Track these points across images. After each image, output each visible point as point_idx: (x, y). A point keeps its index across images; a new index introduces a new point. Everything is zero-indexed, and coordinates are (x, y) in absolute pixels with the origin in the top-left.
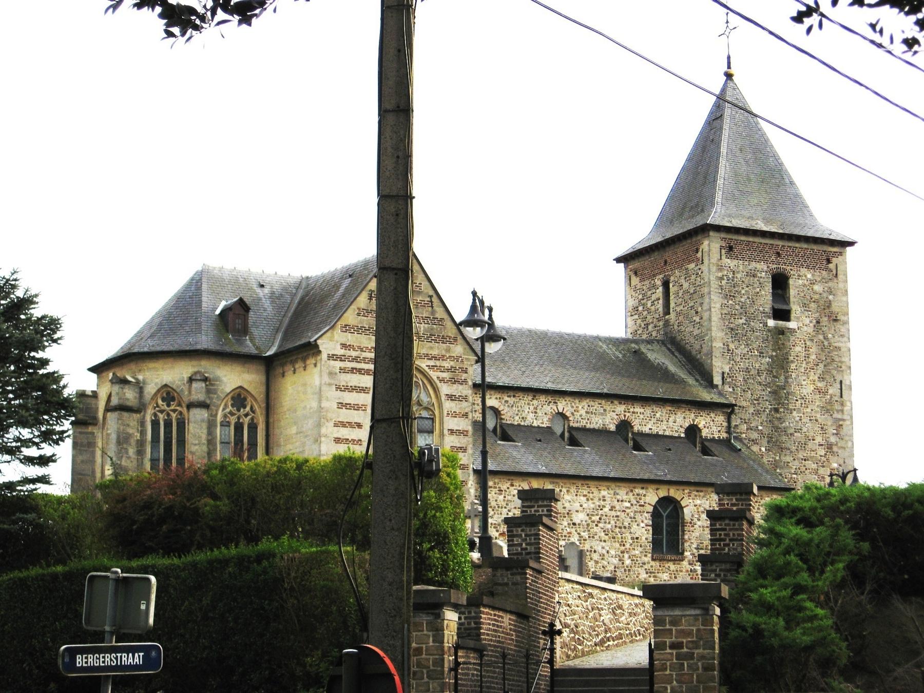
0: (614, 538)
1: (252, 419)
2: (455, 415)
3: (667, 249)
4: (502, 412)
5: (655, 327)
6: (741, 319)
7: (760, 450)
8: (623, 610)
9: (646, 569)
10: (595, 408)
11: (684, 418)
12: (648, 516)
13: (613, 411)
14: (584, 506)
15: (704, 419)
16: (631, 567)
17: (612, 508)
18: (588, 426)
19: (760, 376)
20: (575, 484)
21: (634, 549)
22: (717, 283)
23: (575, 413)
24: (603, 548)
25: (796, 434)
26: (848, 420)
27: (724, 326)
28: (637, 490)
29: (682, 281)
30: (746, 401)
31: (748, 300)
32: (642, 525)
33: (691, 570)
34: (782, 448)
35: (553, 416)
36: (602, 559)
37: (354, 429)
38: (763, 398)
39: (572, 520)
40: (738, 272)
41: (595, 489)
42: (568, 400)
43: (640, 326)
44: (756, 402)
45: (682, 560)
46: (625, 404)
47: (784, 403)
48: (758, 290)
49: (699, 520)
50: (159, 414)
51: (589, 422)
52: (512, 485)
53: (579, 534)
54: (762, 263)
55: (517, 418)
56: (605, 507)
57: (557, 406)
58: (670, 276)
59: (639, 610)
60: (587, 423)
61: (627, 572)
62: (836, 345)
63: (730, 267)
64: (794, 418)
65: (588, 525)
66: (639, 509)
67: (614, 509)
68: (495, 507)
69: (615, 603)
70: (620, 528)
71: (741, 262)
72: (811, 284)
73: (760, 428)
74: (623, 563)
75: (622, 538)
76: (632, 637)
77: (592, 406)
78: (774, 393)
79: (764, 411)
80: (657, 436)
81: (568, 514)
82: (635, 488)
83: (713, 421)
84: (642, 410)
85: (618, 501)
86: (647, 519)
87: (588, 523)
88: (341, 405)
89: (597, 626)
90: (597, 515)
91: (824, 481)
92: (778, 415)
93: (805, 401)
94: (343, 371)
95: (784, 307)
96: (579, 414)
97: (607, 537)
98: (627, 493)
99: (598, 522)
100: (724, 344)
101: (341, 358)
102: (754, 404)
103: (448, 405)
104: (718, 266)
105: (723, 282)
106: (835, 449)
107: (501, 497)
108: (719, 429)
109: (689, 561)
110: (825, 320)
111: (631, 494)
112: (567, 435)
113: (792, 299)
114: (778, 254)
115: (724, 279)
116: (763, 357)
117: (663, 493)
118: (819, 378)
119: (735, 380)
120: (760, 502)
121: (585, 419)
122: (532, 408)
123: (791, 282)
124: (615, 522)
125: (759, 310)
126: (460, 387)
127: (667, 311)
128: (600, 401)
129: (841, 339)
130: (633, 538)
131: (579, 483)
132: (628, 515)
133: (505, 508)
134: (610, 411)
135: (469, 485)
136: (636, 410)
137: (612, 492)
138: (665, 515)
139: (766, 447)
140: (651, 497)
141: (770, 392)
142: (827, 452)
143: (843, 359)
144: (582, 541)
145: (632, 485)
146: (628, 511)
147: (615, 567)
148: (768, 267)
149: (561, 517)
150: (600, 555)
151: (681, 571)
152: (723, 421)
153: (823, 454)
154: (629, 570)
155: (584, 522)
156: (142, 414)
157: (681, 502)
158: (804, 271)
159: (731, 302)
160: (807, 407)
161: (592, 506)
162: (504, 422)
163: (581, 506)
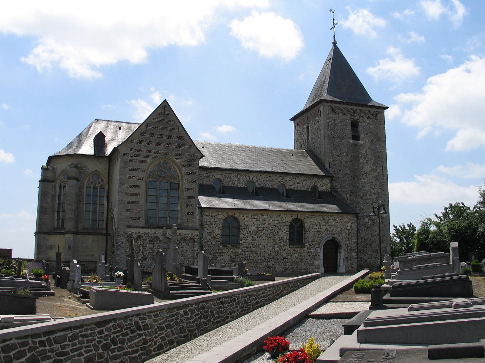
1: (102, 185)
3: (308, 113)
4: (223, 181)
5: (304, 145)
6: (338, 140)
7: (347, 196)
9: (286, 252)
14: (255, 223)
17: (269, 224)
18: (264, 186)
22: (326, 124)
25: (363, 189)
26: (386, 182)
29: (313, 125)
32: (284, 231)
37: (136, 188)
40: (336, 120)
43: (299, 146)
45: (304, 247)
50: (62, 183)
53: (252, 236)
55: (230, 183)
56: (266, 223)
58: (309, 123)
60: (264, 185)
62: (380, 150)
63: (332, 118)
65: (257, 232)
66: (282, 224)
67: (270, 225)
68: (209, 224)
70: (273, 233)
73: (346, 186)
74: (275, 250)
75: (274, 238)
78: (352, 171)
80: (297, 190)
81: (247, 227)
82: (281, 214)
84: (290, 179)
86: (286, 229)
88: (130, 177)
92: (355, 181)
94: (131, 161)
97: (266, 238)
101: (130, 155)
102: (344, 176)
103: (186, 177)
106: (380, 195)
107: (213, 220)
109: (308, 247)
113: (360, 131)
114: (354, 112)
115: (330, 123)
119: (335, 166)
120: (342, 220)
123: (360, 124)
127: (308, 139)
129: (382, 148)
130: (279, 238)
133: (215, 225)
135: (196, 215)
136: (287, 179)
138: (296, 227)
139: (349, 194)
140: (289, 218)
142: (377, 196)
149: (243, 228)
154: (278, 253)
155: (255, 231)
156: (55, 183)
158: (365, 119)
159: (333, 132)
160: (368, 177)
161: (259, 223)
163: (254, 223)
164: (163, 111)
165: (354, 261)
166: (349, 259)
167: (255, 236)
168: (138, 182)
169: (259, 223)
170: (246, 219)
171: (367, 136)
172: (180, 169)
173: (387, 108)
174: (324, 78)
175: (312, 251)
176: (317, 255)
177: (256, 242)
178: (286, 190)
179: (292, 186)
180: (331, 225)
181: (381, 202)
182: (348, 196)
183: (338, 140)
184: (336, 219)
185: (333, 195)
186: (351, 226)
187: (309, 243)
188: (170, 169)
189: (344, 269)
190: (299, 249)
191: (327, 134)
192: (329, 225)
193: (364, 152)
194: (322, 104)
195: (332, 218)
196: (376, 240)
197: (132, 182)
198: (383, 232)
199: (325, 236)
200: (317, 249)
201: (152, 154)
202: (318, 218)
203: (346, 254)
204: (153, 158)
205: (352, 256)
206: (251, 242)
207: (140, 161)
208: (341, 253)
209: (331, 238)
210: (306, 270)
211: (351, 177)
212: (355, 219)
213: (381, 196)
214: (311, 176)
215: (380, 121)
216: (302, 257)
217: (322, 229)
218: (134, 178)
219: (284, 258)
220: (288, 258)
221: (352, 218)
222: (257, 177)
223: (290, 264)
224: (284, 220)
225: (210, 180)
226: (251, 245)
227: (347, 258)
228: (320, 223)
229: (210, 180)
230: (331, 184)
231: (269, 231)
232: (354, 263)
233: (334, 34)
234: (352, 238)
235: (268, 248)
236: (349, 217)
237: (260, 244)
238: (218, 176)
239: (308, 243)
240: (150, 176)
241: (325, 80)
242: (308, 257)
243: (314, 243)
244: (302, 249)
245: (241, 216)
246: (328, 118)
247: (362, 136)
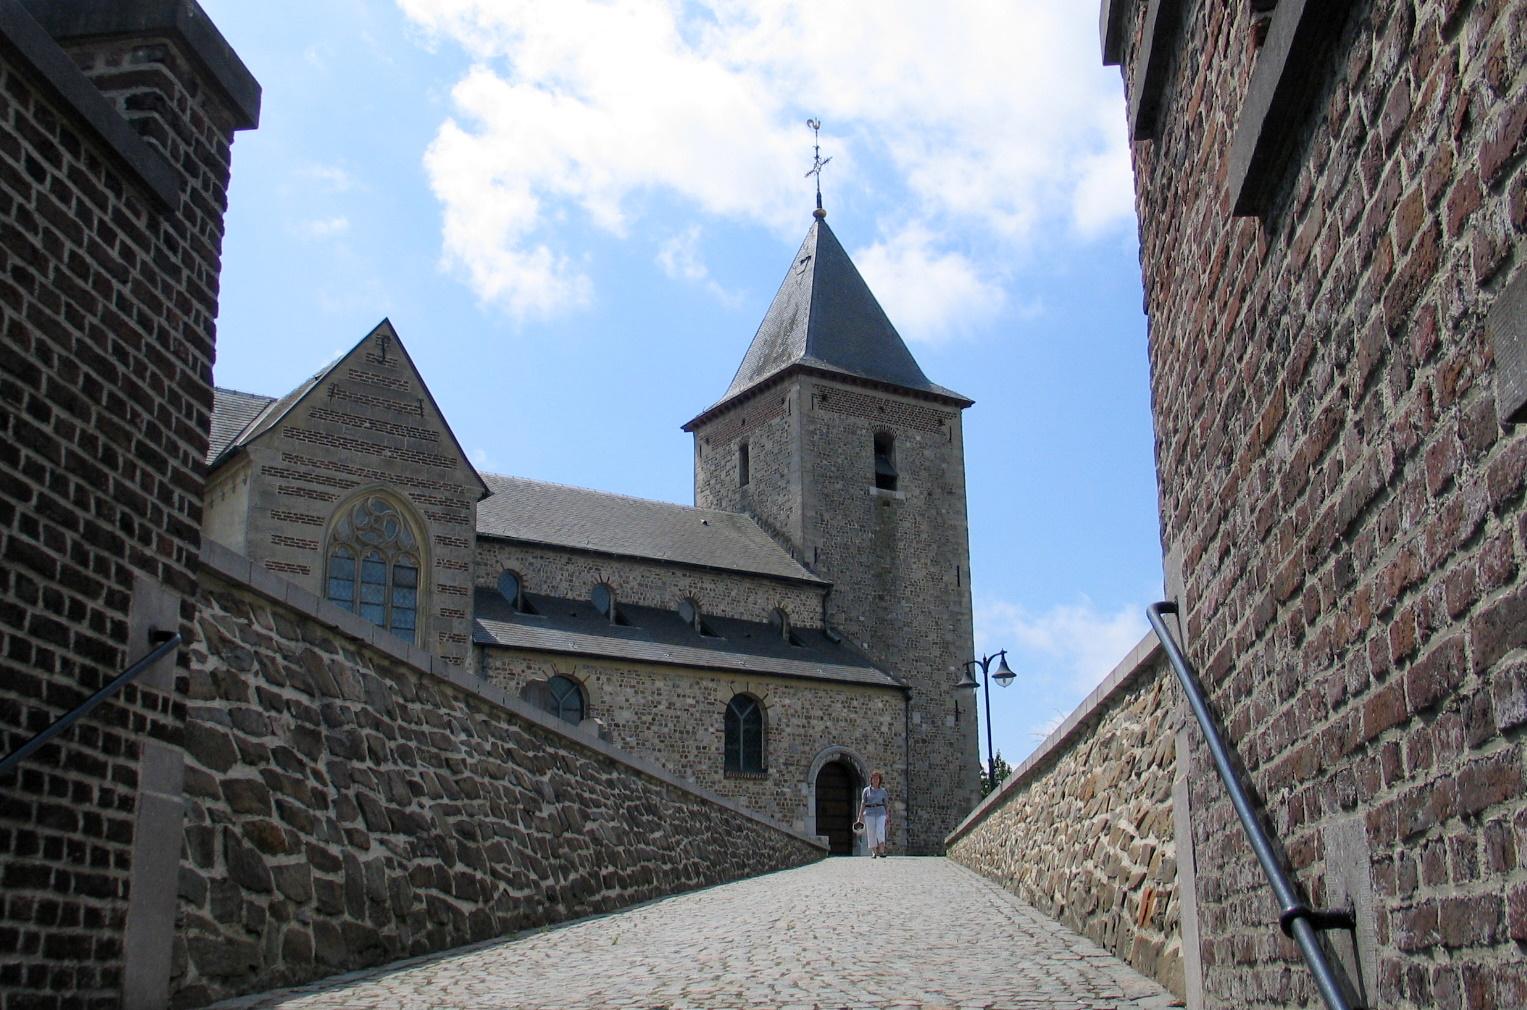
0: (672, 746)
2: (449, 565)
3: (746, 405)
8: (660, 818)
12: (720, 718)
17: (670, 706)
18: (641, 603)
21: (700, 763)
24: (657, 759)
25: (905, 629)
29: (764, 440)
32: (711, 730)
35: (595, 589)
40: (834, 427)
45: (766, 779)
48: (858, 450)
49: (788, 726)
52: (529, 668)
53: (623, 739)
58: (748, 437)
59: (698, 825)
62: (952, 522)
65: (637, 727)
69: (639, 798)
73: (862, 619)
76: (678, 879)
78: (878, 576)
80: (732, 621)
81: (608, 710)
82: (702, 679)
84: (713, 586)
85: (678, 696)
86: (718, 723)
88: (278, 539)
89: (569, 842)
90: (649, 714)
92: (884, 604)
95: (889, 473)
103: (439, 551)
106: (952, 649)
111: (696, 687)
112: (612, 613)
113: (898, 465)
114: (881, 408)
117: (739, 689)
122: (566, 574)
123: (897, 443)
126: (458, 527)
127: (745, 479)
128: (658, 571)
130: (698, 748)
135: (467, 664)
138: (742, 718)
140: (724, 692)
146: (692, 710)
151: (764, 794)
158: (911, 432)
159: (825, 462)
161: (643, 701)
162: (527, 590)
163: (627, 700)
164: (378, 352)
168: (300, 557)
169: (643, 701)
170: (608, 688)
172: (422, 529)
173: (968, 404)
174: (792, 306)
175: (786, 790)
176: (801, 802)
181: (952, 668)
182: (865, 645)
185: (831, 640)
186: (891, 724)
188: (393, 522)
191: (809, 466)
194: (794, 378)
197: (283, 555)
198: (959, 755)
200: (800, 785)
201: (344, 476)
204: (347, 487)
207: (310, 494)
212: (902, 705)
218: (289, 542)
221: (893, 702)
225: (488, 574)
229: (488, 574)
230: (824, 607)
232: (899, 833)
236: (886, 698)
238: (512, 561)
240: (335, 540)
241: (795, 315)
242: (777, 809)
243: (792, 768)
245: (593, 677)
246: (812, 421)
247: (904, 478)
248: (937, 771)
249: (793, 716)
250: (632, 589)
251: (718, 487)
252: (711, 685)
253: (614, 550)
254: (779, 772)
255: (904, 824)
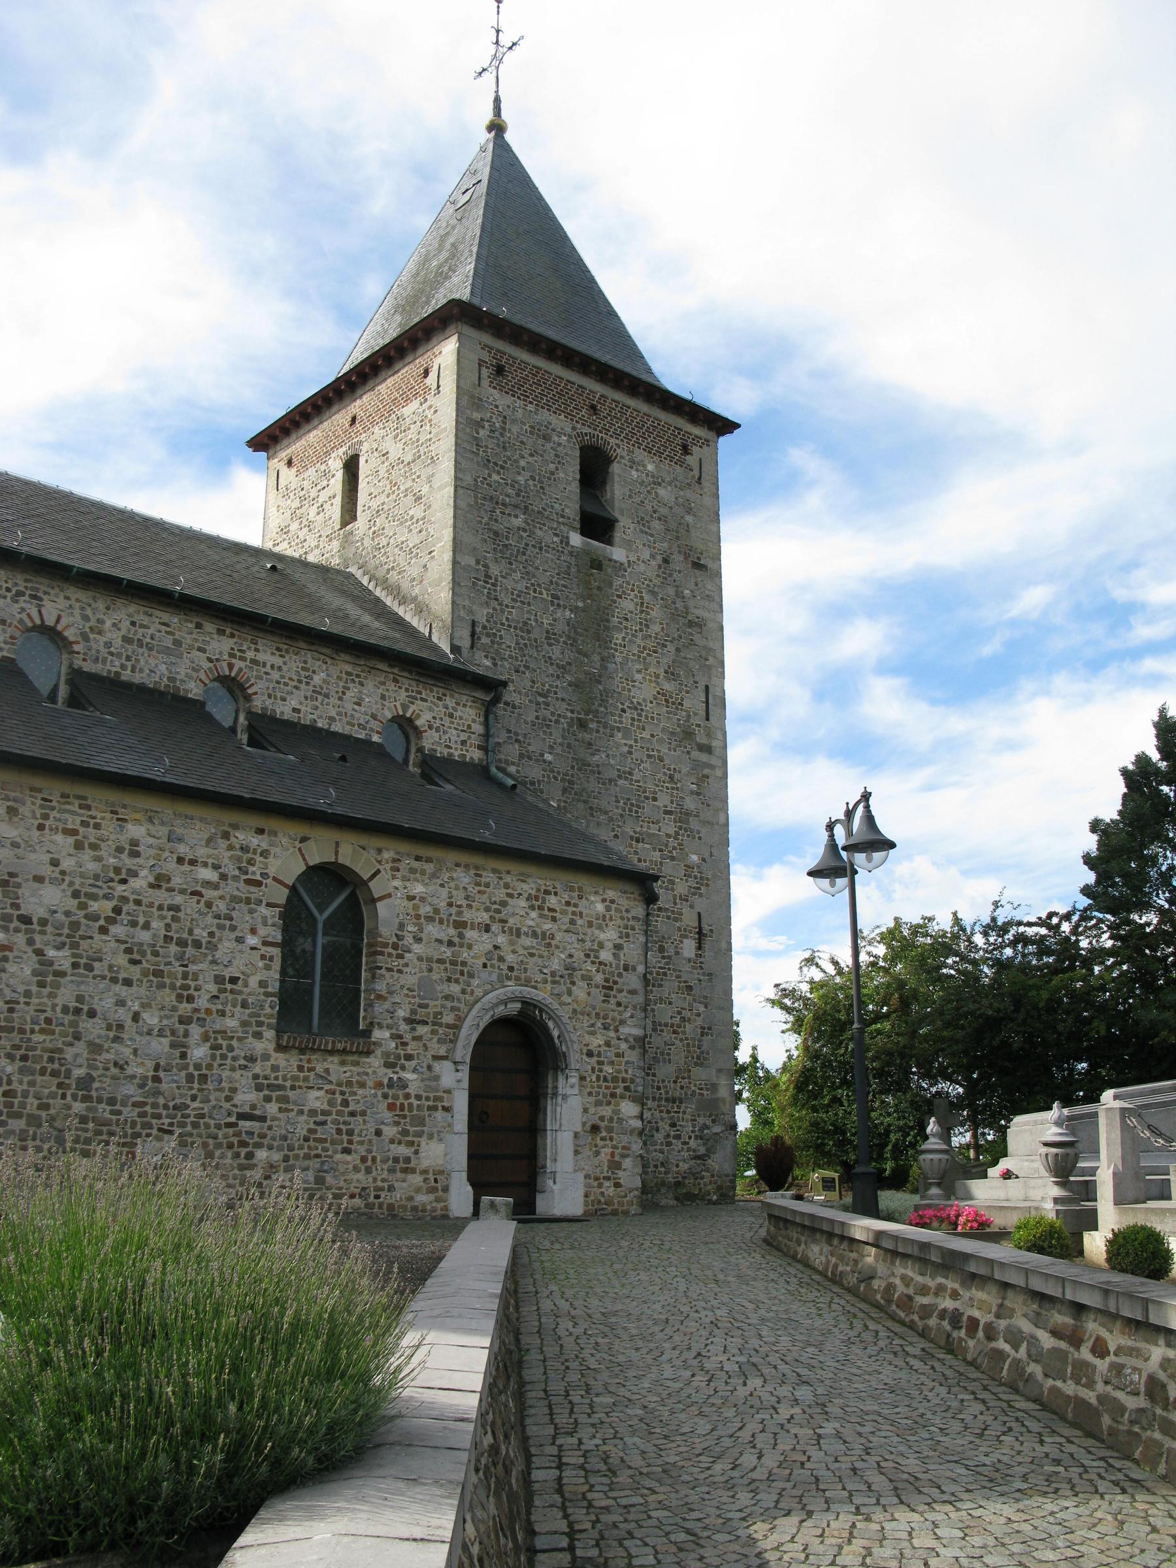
0: (158, 973)
6: (516, 516)
9: (256, 1077)
10: (150, 631)
11: (383, 697)
12: (272, 914)
13: (200, 649)
15: (430, 709)
16: (210, 1067)
18: (126, 675)
19: (550, 645)
20: (40, 791)
21: (222, 1013)
22: (468, 430)
23: (92, 636)
25: (621, 782)
27: (481, 522)
28: (241, 835)
29: (389, 445)
30: (520, 693)
31: (531, 482)
32: (252, 941)
33: (391, 1084)
34: (591, 808)
36: (116, 1039)
38: (556, 693)
39: (16, 906)
40: (514, 421)
41: (108, 815)
42: (73, 597)
44: (541, 700)
45: (368, 1053)
46: (232, 636)
47: (597, 711)
48: (552, 467)
49: (418, 940)
51: (129, 664)
53: (39, 953)
54: (562, 417)
57: (39, 607)
60: (123, 667)
61: (196, 1085)
63: (497, 406)
64: (618, 745)
65: (75, 926)
66: (243, 890)
67: (165, 885)
70: (182, 943)
71: (519, 403)
72: (654, 483)
73: (548, 757)
74: (183, 1056)
75: (185, 976)
77: (142, 626)
79: (557, 722)
82: (236, 827)
83: (451, 716)
84: (278, 661)
85: (180, 860)
87: (74, 918)
90: (106, 897)
91: (673, 890)
93: (640, 715)
96: (103, 639)
97: (135, 972)
98: (209, 841)
99: (108, 919)
100: (478, 562)
102: (538, 704)
104: (472, 397)
105: (482, 432)
106: (694, 824)
108: (464, 736)
110: (677, 558)
111: (223, 844)
112: (63, 691)
114: (593, 407)
115: (483, 427)
116: (558, 605)
118: (666, 672)
120: (576, 905)
121: (119, 655)
123: (615, 468)
124: (168, 927)
125: (552, 507)
127: (349, 512)
128: (166, 617)
130: (219, 980)
131: (54, 788)
132: (209, 905)
134: (191, 647)
136: (261, 657)
137: (163, 831)
138: (321, 918)
141: (570, 684)
143: (711, 645)
144: (50, 979)
145: (229, 817)
146: (209, 894)
147: (157, 1068)
148: (574, 428)
150: (109, 1028)
151: (362, 1085)
152: (474, 721)
153: (671, 831)
154: (203, 1078)
155: (60, 916)
157: (371, 884)
158: (640, 455)
159: (495, 477)
160: (644, 729)
161: (92, 867)
163: (55, 863)
165: (626, 1151)
166: (604, 1134)
167: (60, 954)
171: (646, 533)
175: (409, 1076)
177: (66, 995)
178: (250, 714)
179: (284, 699)
180: (518, 930)
183: (518, 522)
184: (544, 900)
185: (501, 785)
186: (618, 947)
187: (394, 1031)
189: (581, 1199)
190: (336, 1059)
191: (468, 479)
192: (511, 929)
193: (631, 606)
194: (452, 329)
195: (525, 886)
196: (673, 1048)
198: (702, 1008)
199: (486, 993)
200: (437, 1066)
202: (452, 878)
203: (592, 1110)
205: (620, 1120)
206: (27, 994)
208: (565, 1097)
209: (519, 1005)
210: (371, 1199)
211: (569, 714)
212: (639, 910)
213: (699, 832)
214: (391, 666)
215: (700, 478)
216: (352, 1114)
217: (470, 947)
219: (242, 1116)
220: (262, 1119)
221: (624, 902)
222: (89, 612)
223: (277, 1157)
224: (251, 869)
226: (25, 1014)
227: (595, 1129)
228: (459, 913)
230: (486, 724)
231: (154, 925)
233: (497, 92)
234: (620, 1013)
235: (141, 1041)
236: (611, 894)
237: (92, 1014)
239: (389, 1027)
242: (388, 1116)
243: (422, 1030)
244: (357, 1064)
247: (625, 527)
248: (667, 1036)
249: (429, 919)
250: (108, 645)
251: (302, 534)
252: (255, 841)
253: (76, 562)
254: (397, 1037)
255: (637, 1147)
